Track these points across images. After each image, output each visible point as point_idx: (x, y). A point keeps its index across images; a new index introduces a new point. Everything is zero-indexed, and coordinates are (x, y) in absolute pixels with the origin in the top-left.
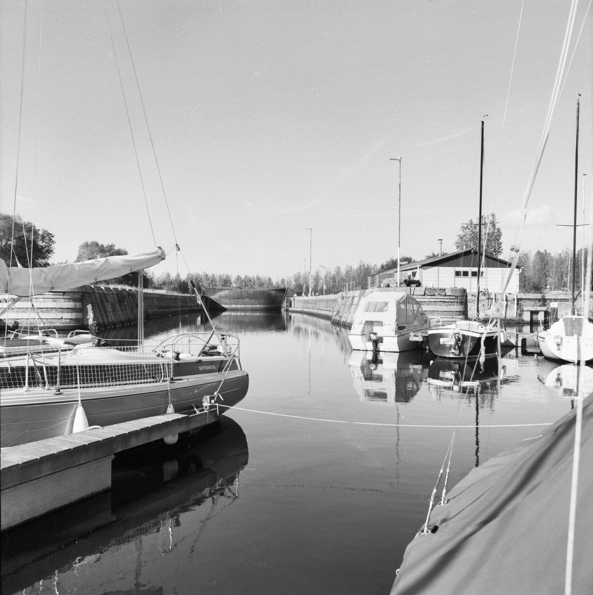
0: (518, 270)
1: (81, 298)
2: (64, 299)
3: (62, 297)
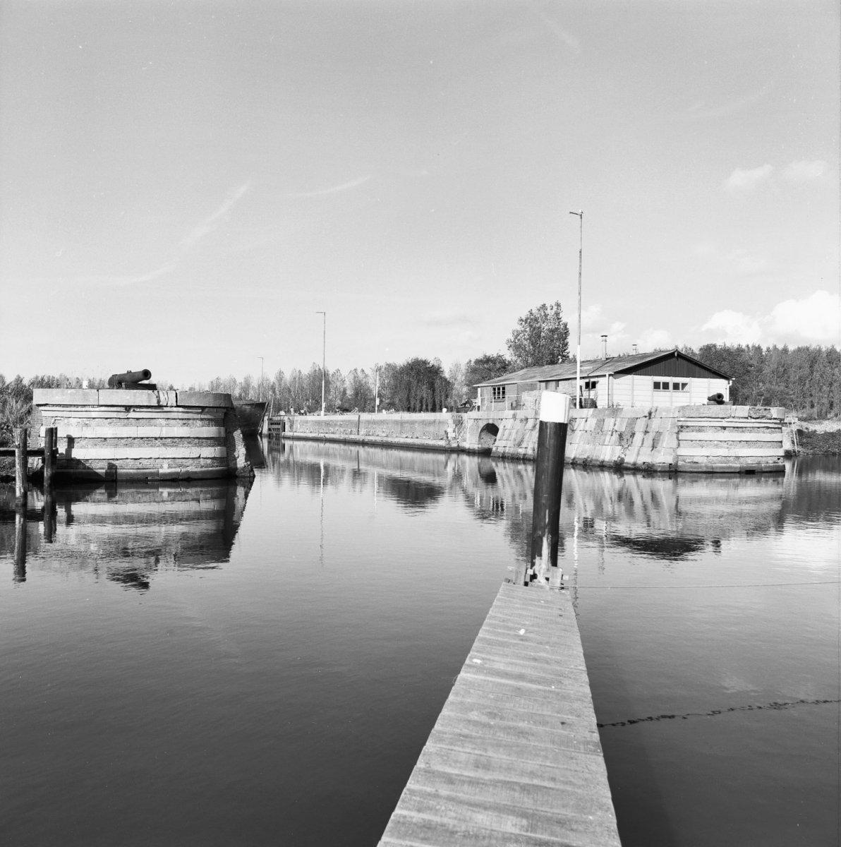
0: (727, 382)
1: (223, 419)
2: (202, 419)
3: (199, 416)
